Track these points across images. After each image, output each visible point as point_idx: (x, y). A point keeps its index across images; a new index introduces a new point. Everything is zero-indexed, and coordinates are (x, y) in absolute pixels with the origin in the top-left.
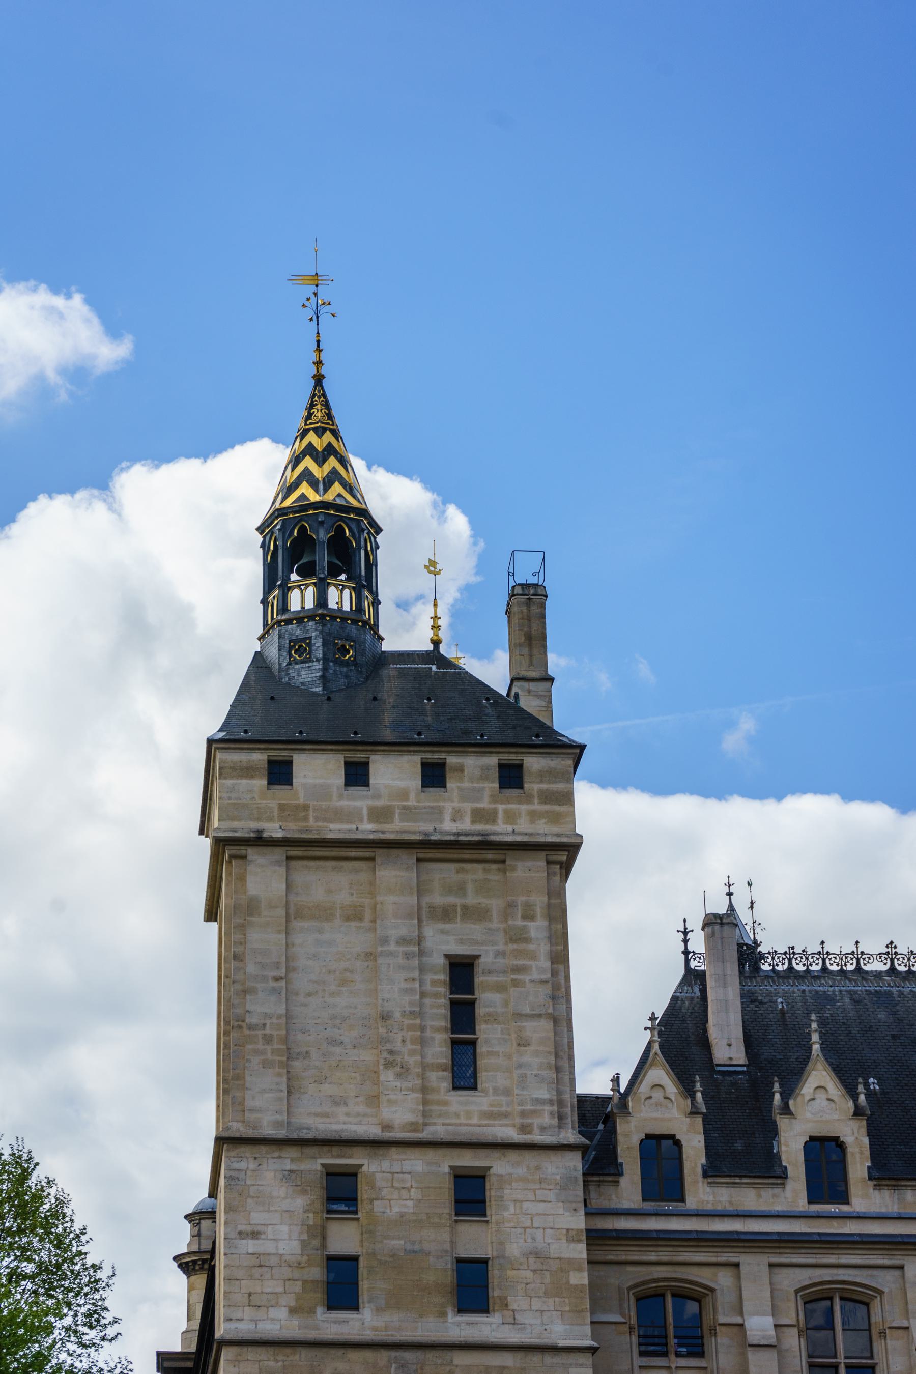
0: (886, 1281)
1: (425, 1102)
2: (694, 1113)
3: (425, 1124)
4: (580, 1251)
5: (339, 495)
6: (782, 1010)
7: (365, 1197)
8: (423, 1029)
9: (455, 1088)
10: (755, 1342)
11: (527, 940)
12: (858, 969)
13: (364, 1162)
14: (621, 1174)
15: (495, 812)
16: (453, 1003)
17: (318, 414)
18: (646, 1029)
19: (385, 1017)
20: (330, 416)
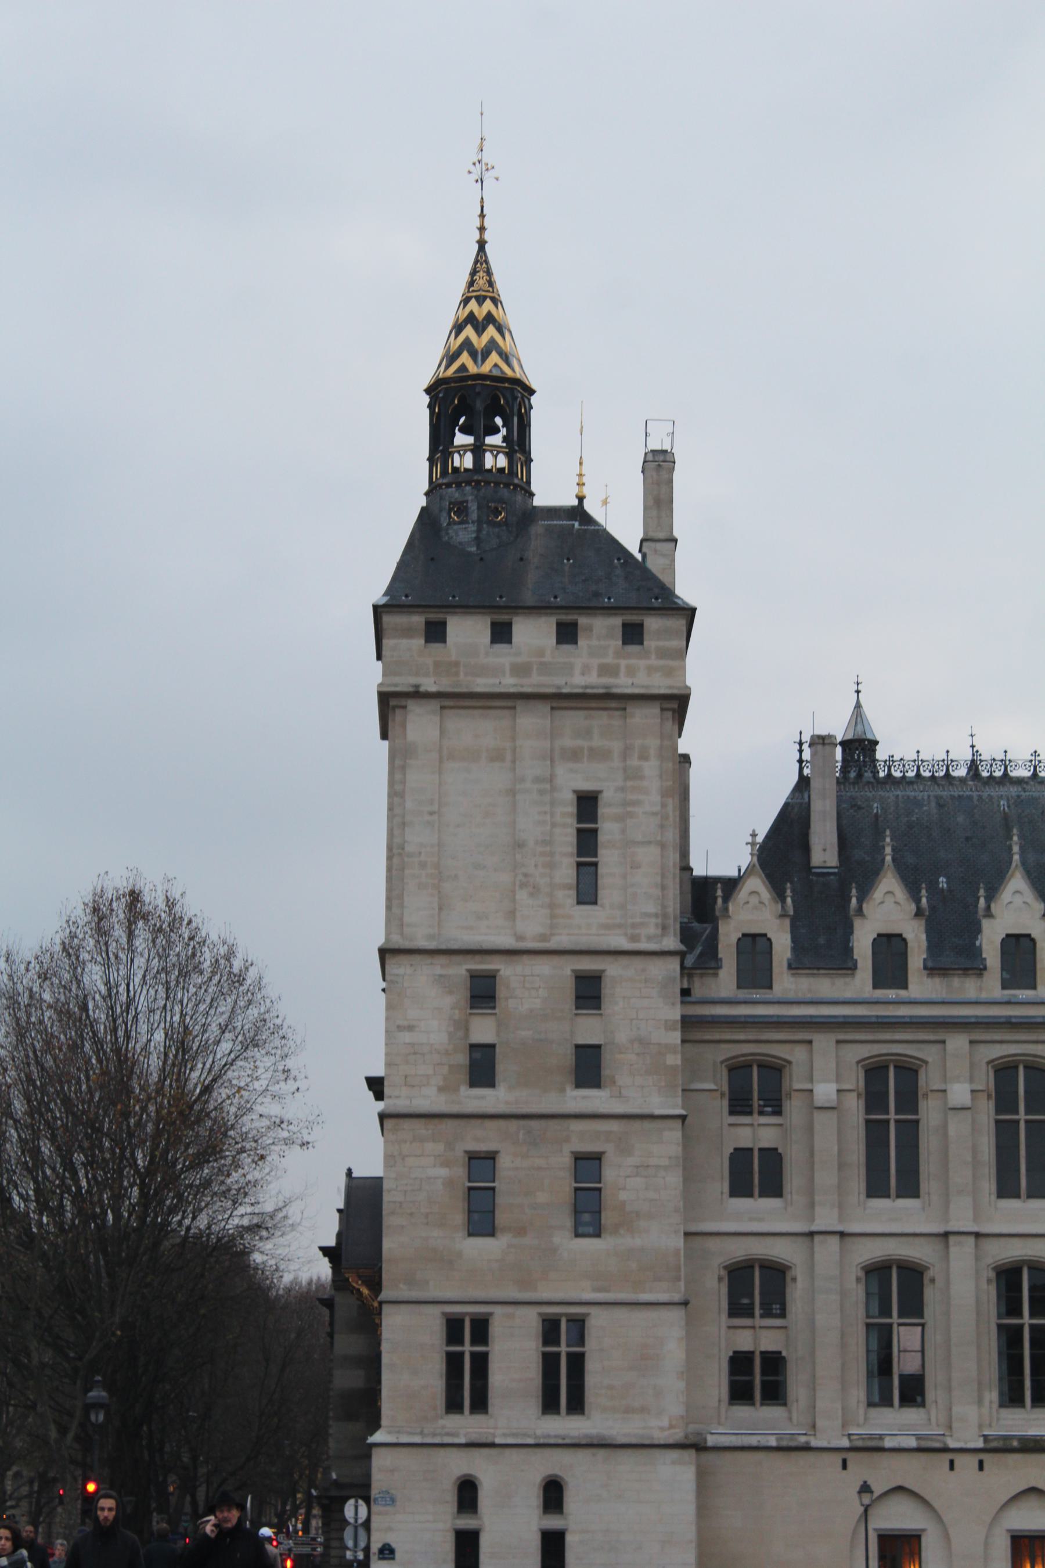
0: (929, 1053)
1: (553, 916)
2: (783, 916)
3: (552, 935)
4: (676, 1037)
5: (496, 365)
6: (876, 814)
7: (502, 996)
8: (552, 854)
9: (579, 903)
10: (820, 1105)
11: (642, 778)
12: (947, 774)
14: (719, 967)
15: (618, 666)
16: (579, 831)
17: (481, 281)
18: (747, 844)
20: (491, 283)
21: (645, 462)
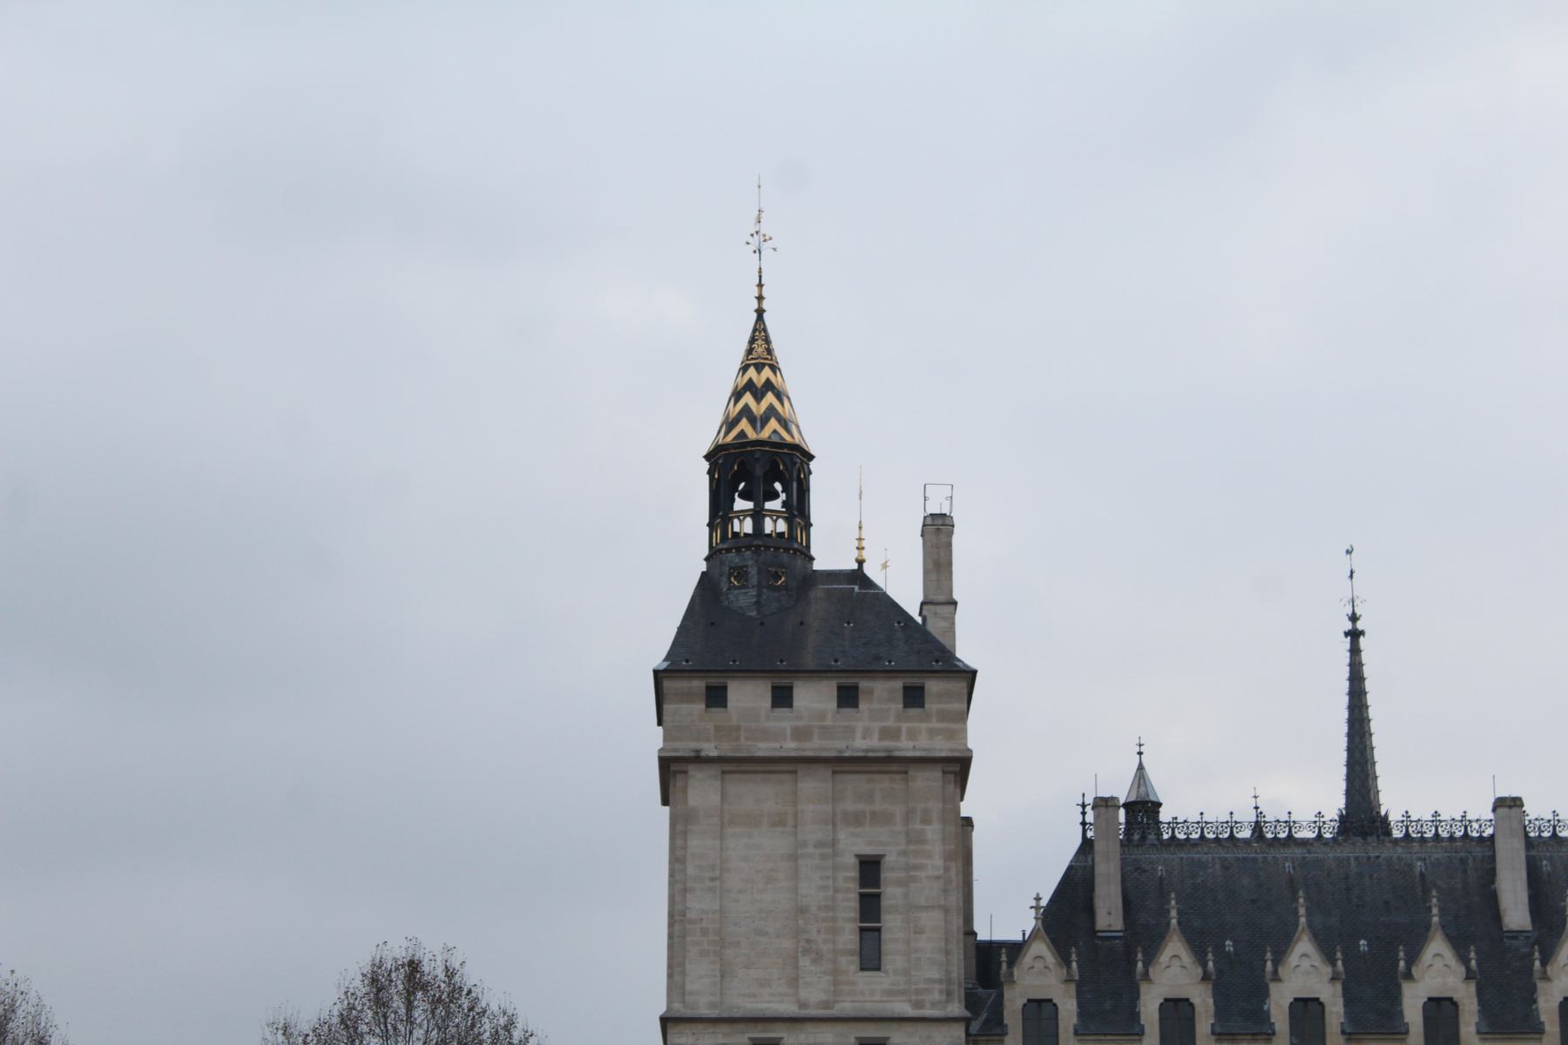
1: (835, 983)
2: (1068, 981)
5: (775, 431)
9: (862, 969)
11: (923, 842)
13: (784, 1035)
15: (899, 730)
16: (862, 896)
17: (760, 349)
19: (802, 910)
20: (769, 351)
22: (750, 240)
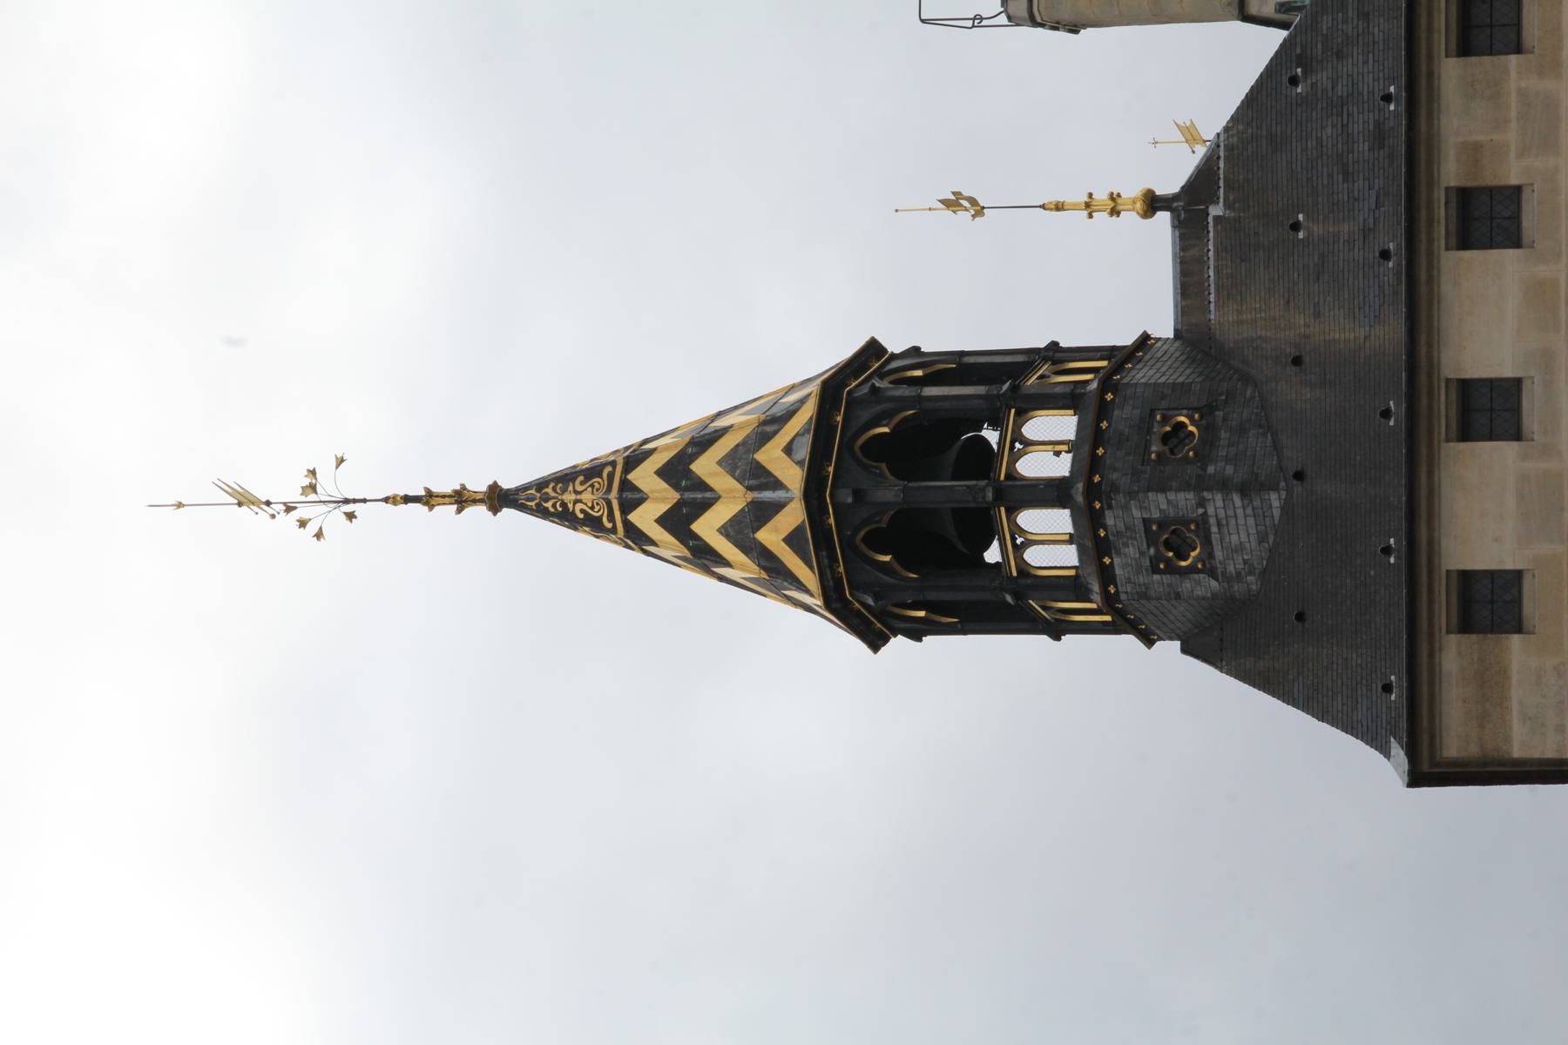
5: (788, 450)
17: (586, 498)
20: (592, 472)
21: (1034, 23)
22: (312, 528)
